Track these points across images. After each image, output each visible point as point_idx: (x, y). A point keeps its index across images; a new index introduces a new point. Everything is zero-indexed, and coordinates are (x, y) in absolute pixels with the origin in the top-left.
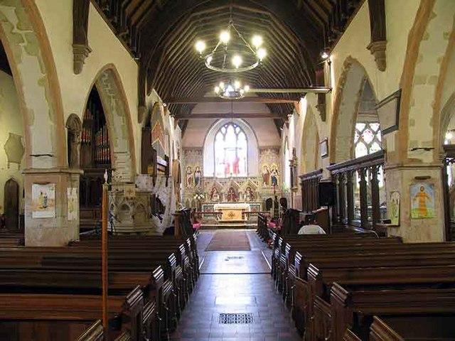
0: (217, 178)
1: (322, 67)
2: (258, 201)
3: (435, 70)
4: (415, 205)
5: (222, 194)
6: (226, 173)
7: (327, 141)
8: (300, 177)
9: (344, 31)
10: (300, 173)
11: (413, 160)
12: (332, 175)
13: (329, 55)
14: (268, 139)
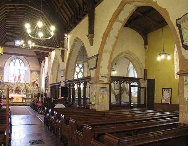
0: (10, 83)
1: (64, 39)
2: (29, 93)
3: (111, 48)
4: (101, 97)
5: (13, 90)
6: (14, 81)
7: (64, 70)
8: (50, 84)
9: (75, 27)
10: (50, 83)
11: (101, 81)
12: (66, 84)
13: (68, 35)
14: (35, 67)
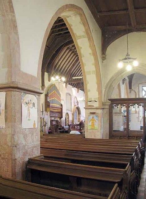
3: (93, 68)
11: (90, 106)
